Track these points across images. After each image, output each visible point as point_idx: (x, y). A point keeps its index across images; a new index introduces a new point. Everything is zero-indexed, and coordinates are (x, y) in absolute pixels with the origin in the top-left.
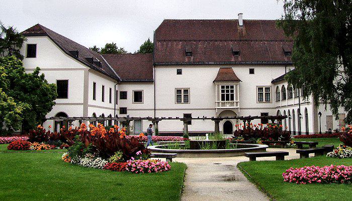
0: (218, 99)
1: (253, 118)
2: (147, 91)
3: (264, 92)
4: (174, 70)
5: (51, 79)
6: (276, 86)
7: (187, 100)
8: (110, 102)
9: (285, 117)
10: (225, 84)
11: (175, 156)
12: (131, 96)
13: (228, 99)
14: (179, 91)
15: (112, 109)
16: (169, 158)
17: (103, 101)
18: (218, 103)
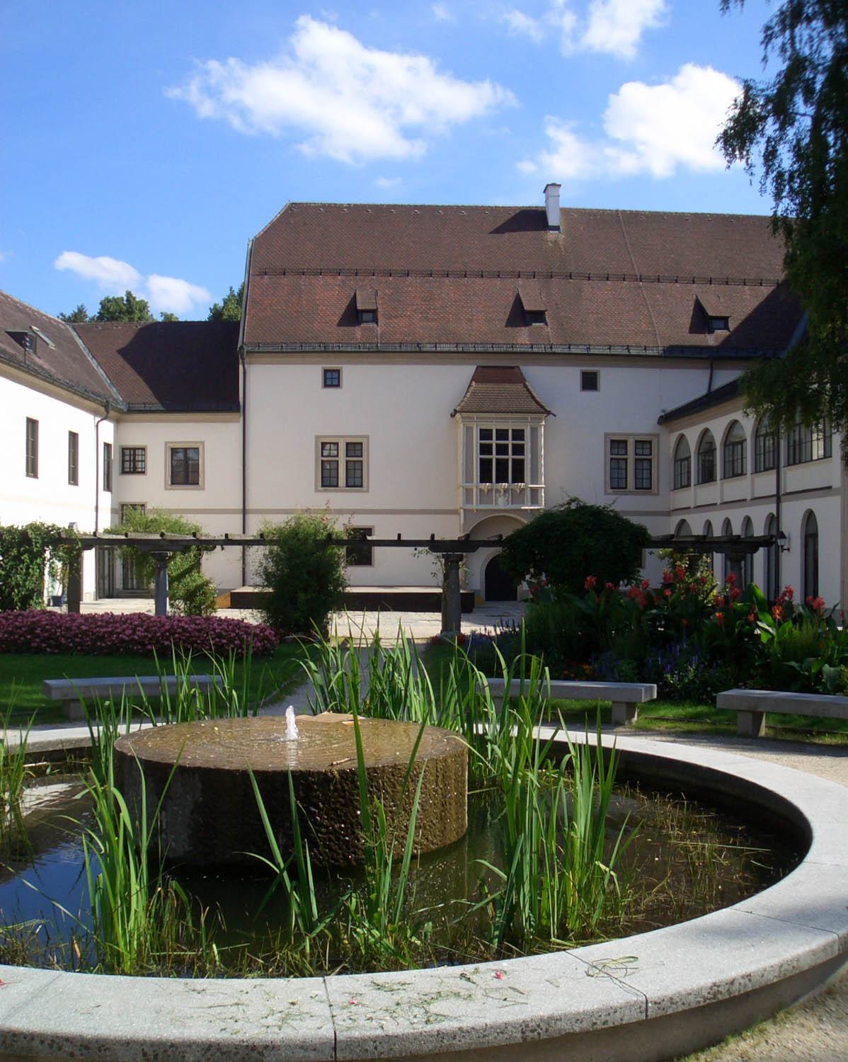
1: (210, 545)
3: (631, 456)
4: (313, 372)
6: (674, 437)
7: (356, 481)
8: (73, 478)
9: (754, 544)
12: (158, 464)
13: (502, 478)
14: (617, 445)
15: (695, 502)
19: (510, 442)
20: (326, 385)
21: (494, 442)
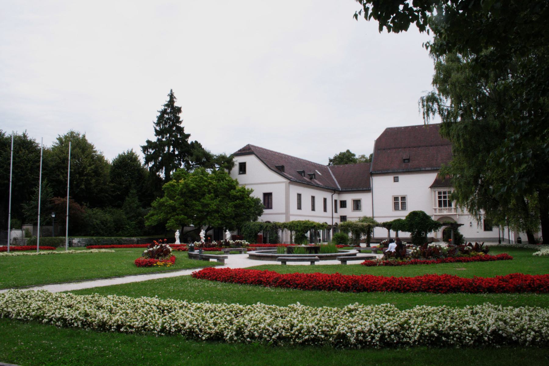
0: (435, 206)
2: (364, 198)
4: (390, 178)
5: (258, 194)
8: (325, 210)
10: (442, 190)
11: (317, 260)
12: (350, 204)
13: (445, 205)
14: (396, 199)
15: (329, 217)
16: (284, 262)
17: (313, 209)
18: (435, 209)
19: (442, 195)
20: (395, 181)
21: (442, 195)
